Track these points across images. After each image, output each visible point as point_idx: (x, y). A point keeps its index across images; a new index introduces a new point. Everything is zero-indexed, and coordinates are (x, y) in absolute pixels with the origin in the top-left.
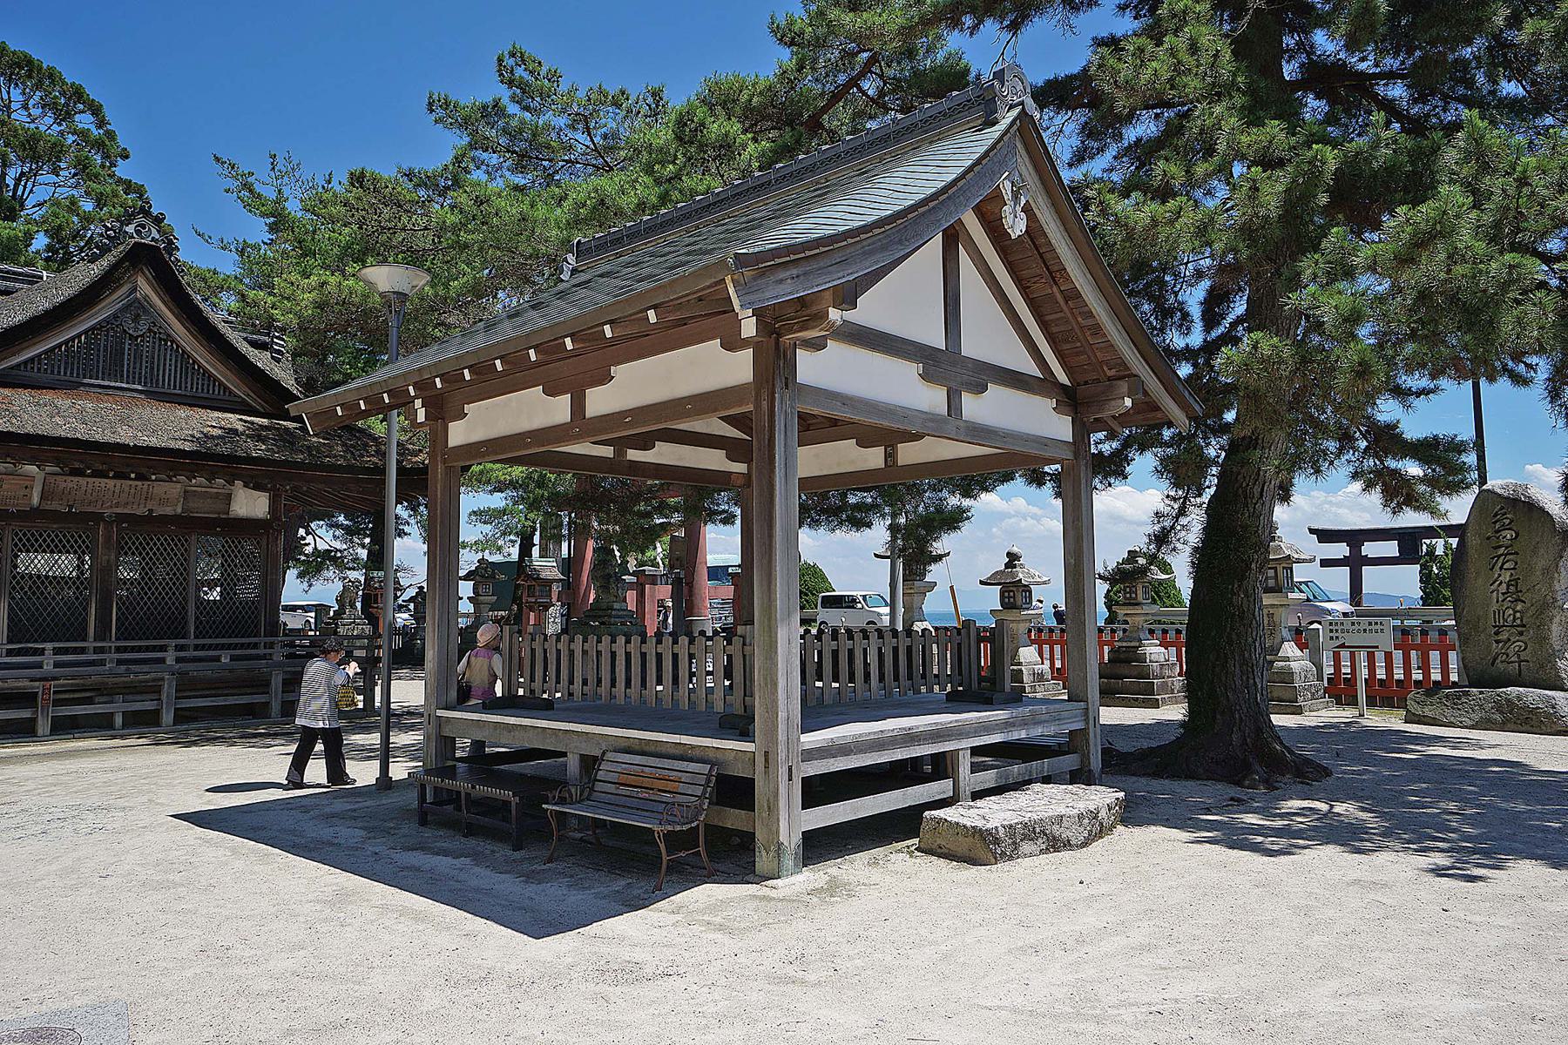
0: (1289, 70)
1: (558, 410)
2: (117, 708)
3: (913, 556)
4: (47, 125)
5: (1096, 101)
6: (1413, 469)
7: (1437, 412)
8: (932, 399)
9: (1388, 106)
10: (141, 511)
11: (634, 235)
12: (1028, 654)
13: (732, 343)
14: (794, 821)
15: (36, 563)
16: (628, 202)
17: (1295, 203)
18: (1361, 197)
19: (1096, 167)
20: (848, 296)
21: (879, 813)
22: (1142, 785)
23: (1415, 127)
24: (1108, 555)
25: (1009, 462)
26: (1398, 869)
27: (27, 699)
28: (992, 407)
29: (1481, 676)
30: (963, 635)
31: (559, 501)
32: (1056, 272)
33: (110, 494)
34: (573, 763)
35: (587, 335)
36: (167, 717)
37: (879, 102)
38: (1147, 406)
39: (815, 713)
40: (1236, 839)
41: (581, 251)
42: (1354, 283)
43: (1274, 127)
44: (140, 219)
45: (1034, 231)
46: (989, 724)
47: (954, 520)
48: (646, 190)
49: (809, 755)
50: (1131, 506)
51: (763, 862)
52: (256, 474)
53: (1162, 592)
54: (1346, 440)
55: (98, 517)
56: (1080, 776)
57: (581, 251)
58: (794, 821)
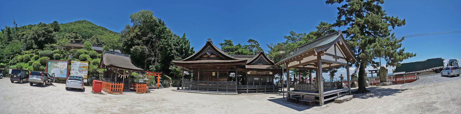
0: (364, 31)
1: (298, 63)
2: (262, 91)
3: (332, 75)
4: (254, 44)
5: (348, 33)
6: (376, 65)
7: (377, 60)
8: (334, 60)
9: (372, 35)
11: (304, 46)
12: (343, 84)
13: (315, 55)
14: (323, 101)
15: (255, 79)
16: (303, 43)
17: (365, 42)
18: (370, 42)
19: (348, 38)
20: (326, 51)
21: (330, 99)
22: (355, 95)
23: (374, 37)
24: (351, 74)
25: (342, 65)
26: (376, 98)
27: (255, 90)
28: (340, 60)
29: (381, 82)
30: (338, 83)
31: (297, 71)
32: (345, 48)
33: (260, 73)
34: (301, 96)
35: (301, 56)
37: (327, 33)
38: (353, 60)
39: (325, 90)
40: (363, 98)
41: (299, 48)
42: (370, 49)
43: (363, 36)
45: (343, 44)
46: (341, 90)
47: (336, 71)
48: (305, 42)
49: (324, 94)
50: (353, 69)
51: (320, 104)
52: (271, 70)
53: (356, 77)
54: (370, 63)
56: (349, 94)
57: (299, 48)
58: (323, 101)
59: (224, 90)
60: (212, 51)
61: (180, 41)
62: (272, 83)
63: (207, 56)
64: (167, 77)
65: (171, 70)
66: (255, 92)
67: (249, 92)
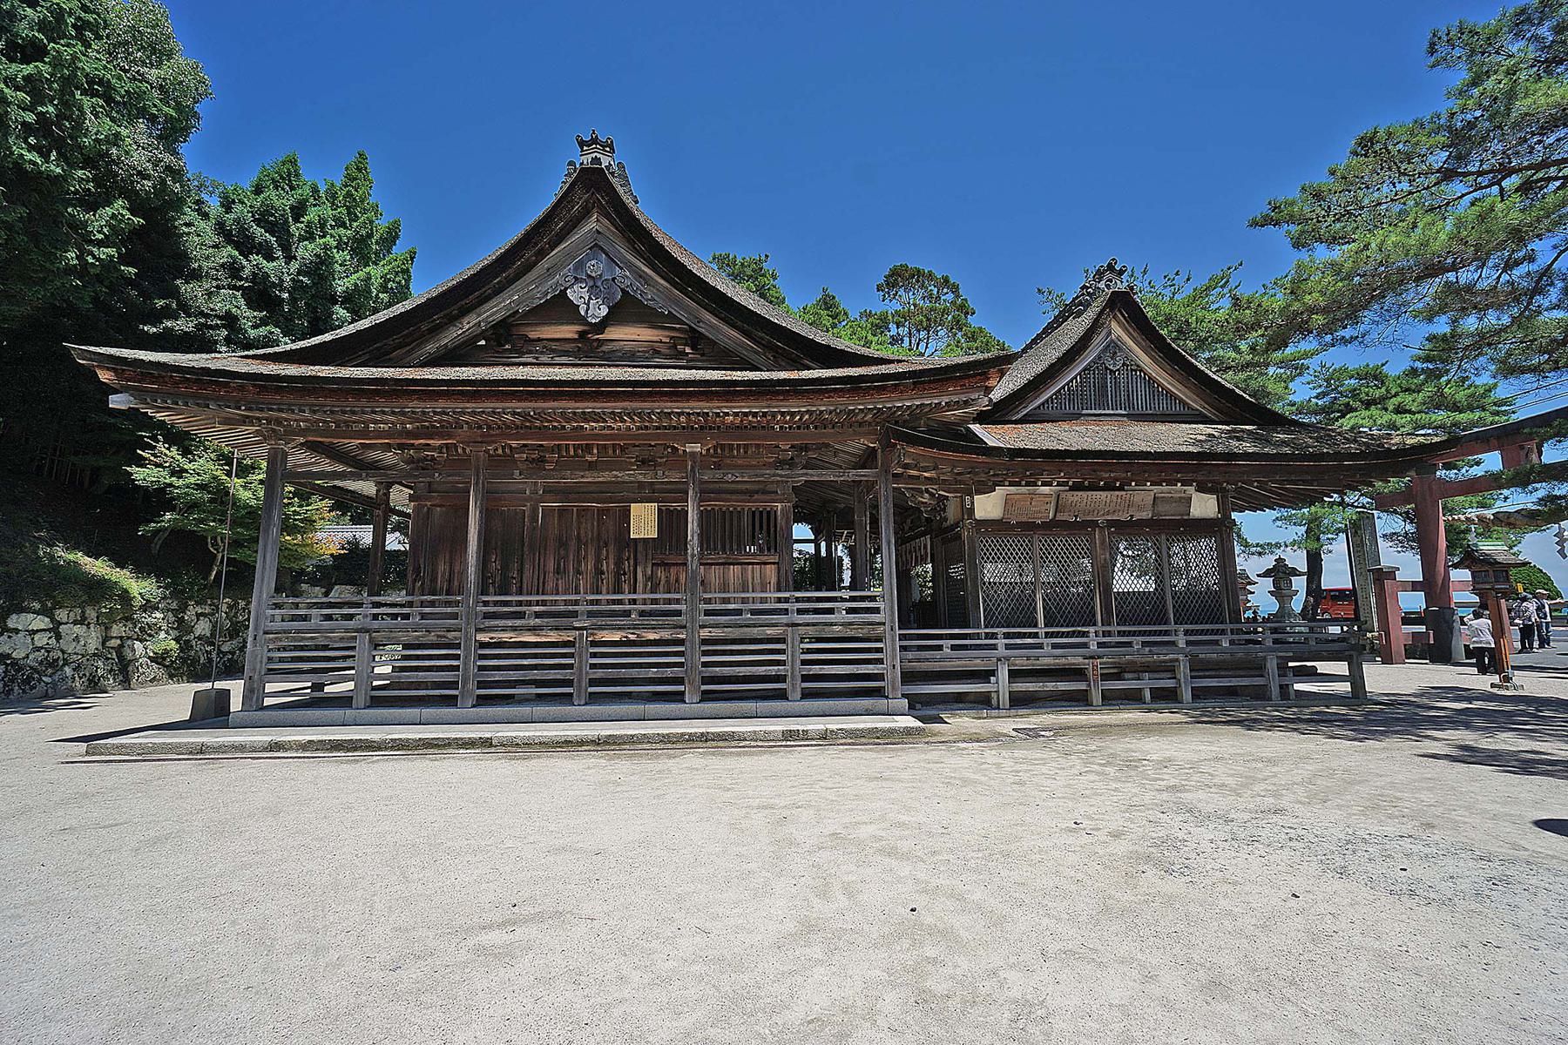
2: (1146, 684)
10: (1124, 517)
27: (1077, 673)
36: (1187, 695)
44: (1108, 275)
55: (1094, 524)
59: (765, 691)
60: (624, 277)
61: (299, 211)
62: (1219, 604)
63: (568, 331)
64: (99, 567)
65: (159, 499)
66: (1080, 700)
67: (1020, 701)
